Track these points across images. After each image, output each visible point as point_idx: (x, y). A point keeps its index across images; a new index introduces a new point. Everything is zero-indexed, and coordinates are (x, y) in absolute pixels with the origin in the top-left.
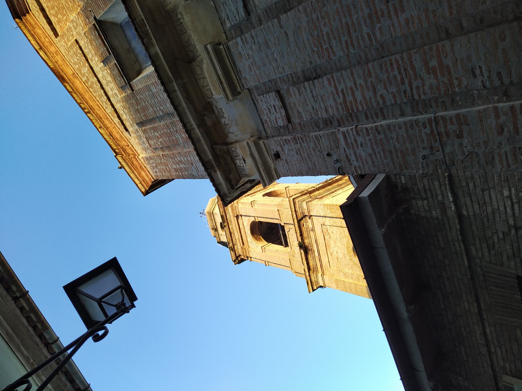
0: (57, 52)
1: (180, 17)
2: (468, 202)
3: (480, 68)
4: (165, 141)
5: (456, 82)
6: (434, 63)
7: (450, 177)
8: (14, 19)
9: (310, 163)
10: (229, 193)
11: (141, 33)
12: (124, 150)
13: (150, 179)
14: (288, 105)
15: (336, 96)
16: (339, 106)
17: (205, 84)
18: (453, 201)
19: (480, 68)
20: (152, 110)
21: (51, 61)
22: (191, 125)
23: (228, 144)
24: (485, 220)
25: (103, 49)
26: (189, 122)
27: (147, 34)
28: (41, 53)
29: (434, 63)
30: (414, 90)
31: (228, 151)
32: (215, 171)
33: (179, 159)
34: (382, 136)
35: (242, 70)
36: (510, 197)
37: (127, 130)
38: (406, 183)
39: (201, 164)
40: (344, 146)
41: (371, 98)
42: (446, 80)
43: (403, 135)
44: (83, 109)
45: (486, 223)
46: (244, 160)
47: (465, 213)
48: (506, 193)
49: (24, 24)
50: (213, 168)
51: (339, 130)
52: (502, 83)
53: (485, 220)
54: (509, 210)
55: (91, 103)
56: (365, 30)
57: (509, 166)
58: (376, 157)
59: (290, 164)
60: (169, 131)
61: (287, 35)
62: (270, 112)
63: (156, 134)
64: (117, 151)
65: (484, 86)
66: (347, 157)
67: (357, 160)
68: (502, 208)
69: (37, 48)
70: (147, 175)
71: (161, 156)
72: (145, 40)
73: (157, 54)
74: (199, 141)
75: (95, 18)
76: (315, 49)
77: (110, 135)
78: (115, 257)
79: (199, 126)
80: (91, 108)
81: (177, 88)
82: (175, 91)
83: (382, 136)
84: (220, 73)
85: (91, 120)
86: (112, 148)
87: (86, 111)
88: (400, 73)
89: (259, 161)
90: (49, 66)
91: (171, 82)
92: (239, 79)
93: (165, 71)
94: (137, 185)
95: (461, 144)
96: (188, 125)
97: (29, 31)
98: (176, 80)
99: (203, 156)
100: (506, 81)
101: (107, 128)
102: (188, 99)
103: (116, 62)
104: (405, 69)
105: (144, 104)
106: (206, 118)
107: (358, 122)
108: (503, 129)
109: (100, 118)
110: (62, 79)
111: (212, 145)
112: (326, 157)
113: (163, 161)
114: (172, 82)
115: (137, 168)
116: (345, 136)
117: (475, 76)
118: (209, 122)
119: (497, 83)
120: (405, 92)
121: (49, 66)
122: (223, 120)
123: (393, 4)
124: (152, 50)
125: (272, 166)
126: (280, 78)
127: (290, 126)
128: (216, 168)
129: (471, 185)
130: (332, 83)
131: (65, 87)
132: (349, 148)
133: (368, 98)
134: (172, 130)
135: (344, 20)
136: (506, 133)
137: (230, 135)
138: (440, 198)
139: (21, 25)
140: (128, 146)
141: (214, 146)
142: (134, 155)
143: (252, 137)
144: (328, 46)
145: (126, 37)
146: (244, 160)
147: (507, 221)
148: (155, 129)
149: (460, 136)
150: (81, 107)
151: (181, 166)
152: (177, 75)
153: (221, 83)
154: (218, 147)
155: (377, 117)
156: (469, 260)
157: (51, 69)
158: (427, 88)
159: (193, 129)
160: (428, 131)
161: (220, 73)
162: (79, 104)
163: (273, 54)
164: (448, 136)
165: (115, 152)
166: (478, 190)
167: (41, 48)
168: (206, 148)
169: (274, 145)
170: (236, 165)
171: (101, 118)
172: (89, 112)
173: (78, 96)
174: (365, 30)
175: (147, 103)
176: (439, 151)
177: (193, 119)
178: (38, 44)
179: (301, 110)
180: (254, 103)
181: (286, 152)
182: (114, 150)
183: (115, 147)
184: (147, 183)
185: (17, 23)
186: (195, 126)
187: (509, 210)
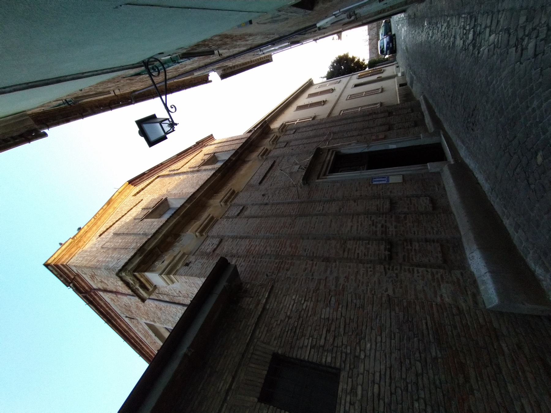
0: (122, 199)
2: (273, 301)
3: (308, 249)
5: (297, 252)
6: (294, 245)
7: (273, 287)
10: (129, 271)
14: (221, 245)
15: (248, 246)
18: (266, 298)
19: (308, 249)
24: (276, 312)
25: (152, 205)
28: (117, 193)
29: (294, 245)
30: (281, 251)
32: (140, 256)
34: (255, 264)
36: (294, 300)
37: (100, 236)
38: (248, 288)
39: (146, 240)
41: (261, 250)
42: (294, 251)
45: (275, 314)
47: (268, 307)
48: (294, 297)
49: (126, 186)
50: (142, 253)
52: (313, 255)
53: (276, 312)
54: (291, 307)
56: (277, 229)
57: (301, 285)
64: (75, 238)
65: (307, 255)
68: (288, 306)
74: (155, 239)
78: (311, 79)
79: (164, 235)
81: (177, 218)
82: (175, 218)
83: (255, 264)
88: (280, 245)
91: (178, 215)
92: (209, 230)
93: (181, 212)
95: (286, 273)
96: (161, 230)
99: (147, 245)
100: (315, 255)
102: (175, 225)
104: (282, 244)
108: (306, 270)
111: (158, 246)
115: (69, 251)
117: (305, 251)
119: (312, 255)
120: (277, 251)
121: (112, 197)
124: (186, 204)
129: (280, 292)
131: (104, 206)
136: (306, 271)
138: (260, 298)
140: (85, 242)
147: (287, 313)
149: (287, 270)
150: (96, 214)
152: (183, 216)
153: (201, 226)
156: (250, 340)
158: (286, 252)
160: (276, 266)
161: (205, 223)
164: (283, 269)
166: (282, 295)
168: (153, 244)
174: (277, 229)
176: (275, 275)
177: (167, 231)
186: (163, 233)
187: (291, 307)
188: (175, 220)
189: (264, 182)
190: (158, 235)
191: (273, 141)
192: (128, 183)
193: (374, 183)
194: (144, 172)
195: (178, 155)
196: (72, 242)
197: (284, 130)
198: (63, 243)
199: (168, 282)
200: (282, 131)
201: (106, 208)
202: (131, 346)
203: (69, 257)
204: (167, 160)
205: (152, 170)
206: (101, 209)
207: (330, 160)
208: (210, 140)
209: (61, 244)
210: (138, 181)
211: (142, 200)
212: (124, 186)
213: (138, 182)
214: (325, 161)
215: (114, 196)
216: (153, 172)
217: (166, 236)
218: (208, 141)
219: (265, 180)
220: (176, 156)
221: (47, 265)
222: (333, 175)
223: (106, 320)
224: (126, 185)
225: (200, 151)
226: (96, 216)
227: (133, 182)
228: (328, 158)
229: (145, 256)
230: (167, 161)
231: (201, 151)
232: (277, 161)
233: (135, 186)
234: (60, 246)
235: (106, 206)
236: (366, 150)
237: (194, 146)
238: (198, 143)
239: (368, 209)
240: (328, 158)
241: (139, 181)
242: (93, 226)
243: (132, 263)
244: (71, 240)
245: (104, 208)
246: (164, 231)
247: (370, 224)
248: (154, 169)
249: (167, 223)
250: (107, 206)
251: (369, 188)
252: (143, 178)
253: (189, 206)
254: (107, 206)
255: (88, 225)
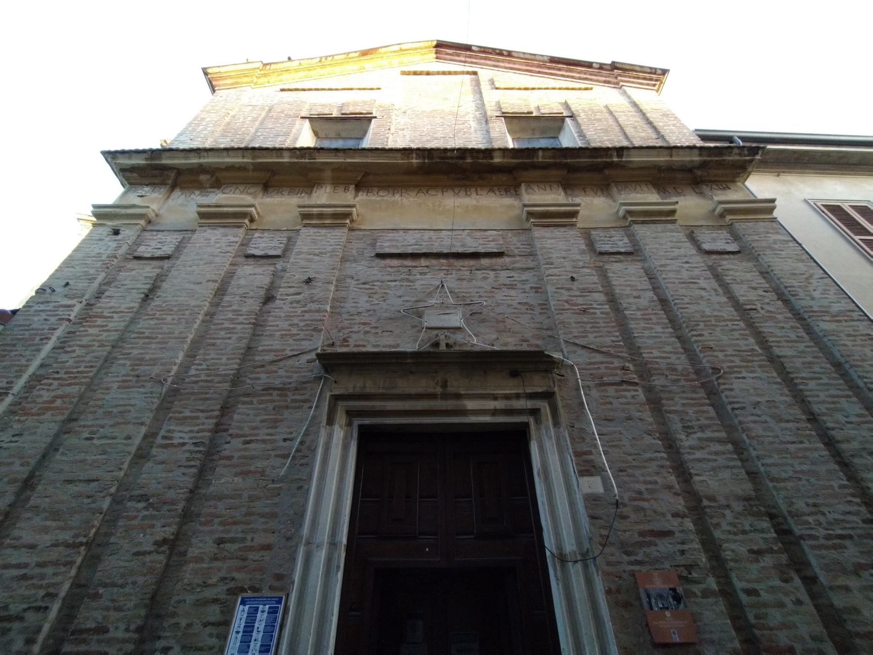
1: (303, 195)
4: (236, 124)
8: (437, 41)
9: (77, 263)
11: (305, 151)
12: (265, 75)
13: (219, 86)
15: (113, 310)
16: (101, 310)
17: (237, 191)
20: (270, 126)
21: (385, 53)
22: (204, 157)
23: (173, 188)
26: (208, 157)
27: (302, 157)
31: (165, 184)
32: (146, 159)
33: (209, 129)
35: (215, 231)
40: (61, 303)
43: (19, 361)
44: (326, 57)
46: (142, 196)
49: (426, 48)
51: (81, 302)
55: (329, 69)
58: (22, 330)
59: (96, 242)
60: (240, 133)
61: (198, 284)
62: (159, 243)
63: (250, 118)
64: (268, 67)
66: (48, 302)
67: (36, 311)
69: (403, 47)
70: (226, 85)
71: (229, 111)
72: (298, 152)
73: (282, 157)
74: (186, 158)
75: (375, 117)
76: (164, 305)
77: (287, 70)
79: (201, 165)
80: (324, 66)
81: (245, 160)
82: (243, 157)
84: (225, 209)
85: (312, 59)
86: (274, 63)
87: (324, 59)
89: (123, 211)
90: (381, 47)
93: (265, 157)
94: (219, 67)
96: (205, 154)
97: (421, 48)
98: (253, 164)
99: (168, 154)
101: (296, 71)
102: (231, 168)
103: (534, 115)
105: (281, 121)
106: (208, 177)
107: (74, 324)
109: (309, 69)
110: (365, 53)
111: (179, 171)
112: (67, 281)
113: (224, 110)
114: (253, 159)
115: (239, 77)
116: (69, 306)
118: (203, 178)
121: (381, 47)
122: (197, 192)
123: (130, 381)
124: (286, 154)
125: (109, 223)
126: (282, 277)
127: (131, 257)
128: (149, 162)
130: (126, 310)
131: (356, 52)
132: (54, 307)
133: (83, 338)
134: (238, 136)
135: (160, 336)
137: (180, 193)
139: (429, 43)
141: (176, 171)
142: (256, 84)
143: (157, 215)
144: (157, 316)
145: (351, 138)
146: (142, 196)
148: (254, 120)
150: (330, 56)
151: (201, 127)
152: (259, 167)
154: (173, 175)
155: (61, 343)
157: (378, 48)
159: (200, 158)
161: (225, 209)
162: (333, 56)
163: (198, 265)
165: (267, 64)
167: (401, 50)
169: (129, 234)
170: (147, 185)
171: (309, 70)
172: (320, 61)
173: (341, 59)
175: (278, 125)
178: (406, 50)
179: (133, 273)
180: (182, 231)
181: (110, 243)
182: (270, 64)
183: (273, 67)
184: (216, 80)
185: (432, 41)
186: (202, 161)
188: (240, 160)
189: (388, 262)
190: (195, 157)
191: (629, 213)
192: (435, 43)
193: (241, 614)
194: (471, 46)
195: (554, 60)
196: (258, 68)
197: (728, 218)
198: (292, 58)
199: (563, 208)
200: (722, 216)
201: (353, 58)
202: (850, 174)
203: (232, 84)
204: (524, 53)
205: (484, 52)
206: (345, 54)
207: (464, 412)
208: (645, 79)
209: (289, 59)
210: (448, 54)
211: (282, 90)
212: (422, 45)
213: (447, 56)
214: (458, 396)
215: (387, 48)
216: (482, 58)
217: (202, 169)
218: (638, 78)
219: (396, 262)
220: (546, 59)
221: (664, 72)
222: (346, 447)
223: (636, 158)
224: (427, 44)
225: (583, 86)
226: (326, 59)
227: (440, 45)
228: (470, 405)
229: (151, 165)
230: (522, 56)
231: (586, 89)
232: (507, 260)
233: (437, 58)
234: (287, 60)
235: (357, 54)
236: (548, 553)
237: (602, 67)
238: (614, 66)
239: (96, 596)
240: (470, 405)
241: (451, 54)
242: (305, 69)
243: (130, 158)
244: (260, 65)
245: (351, 55)
246: (206, 160)
247: (11, 606)
248: (491, 53)
249: (225, 154)
250: (359, 56)
251: (219, 591)
252: (458, 55)
253: (286, 160)
254: (359, 56)
255: (301, 61)
